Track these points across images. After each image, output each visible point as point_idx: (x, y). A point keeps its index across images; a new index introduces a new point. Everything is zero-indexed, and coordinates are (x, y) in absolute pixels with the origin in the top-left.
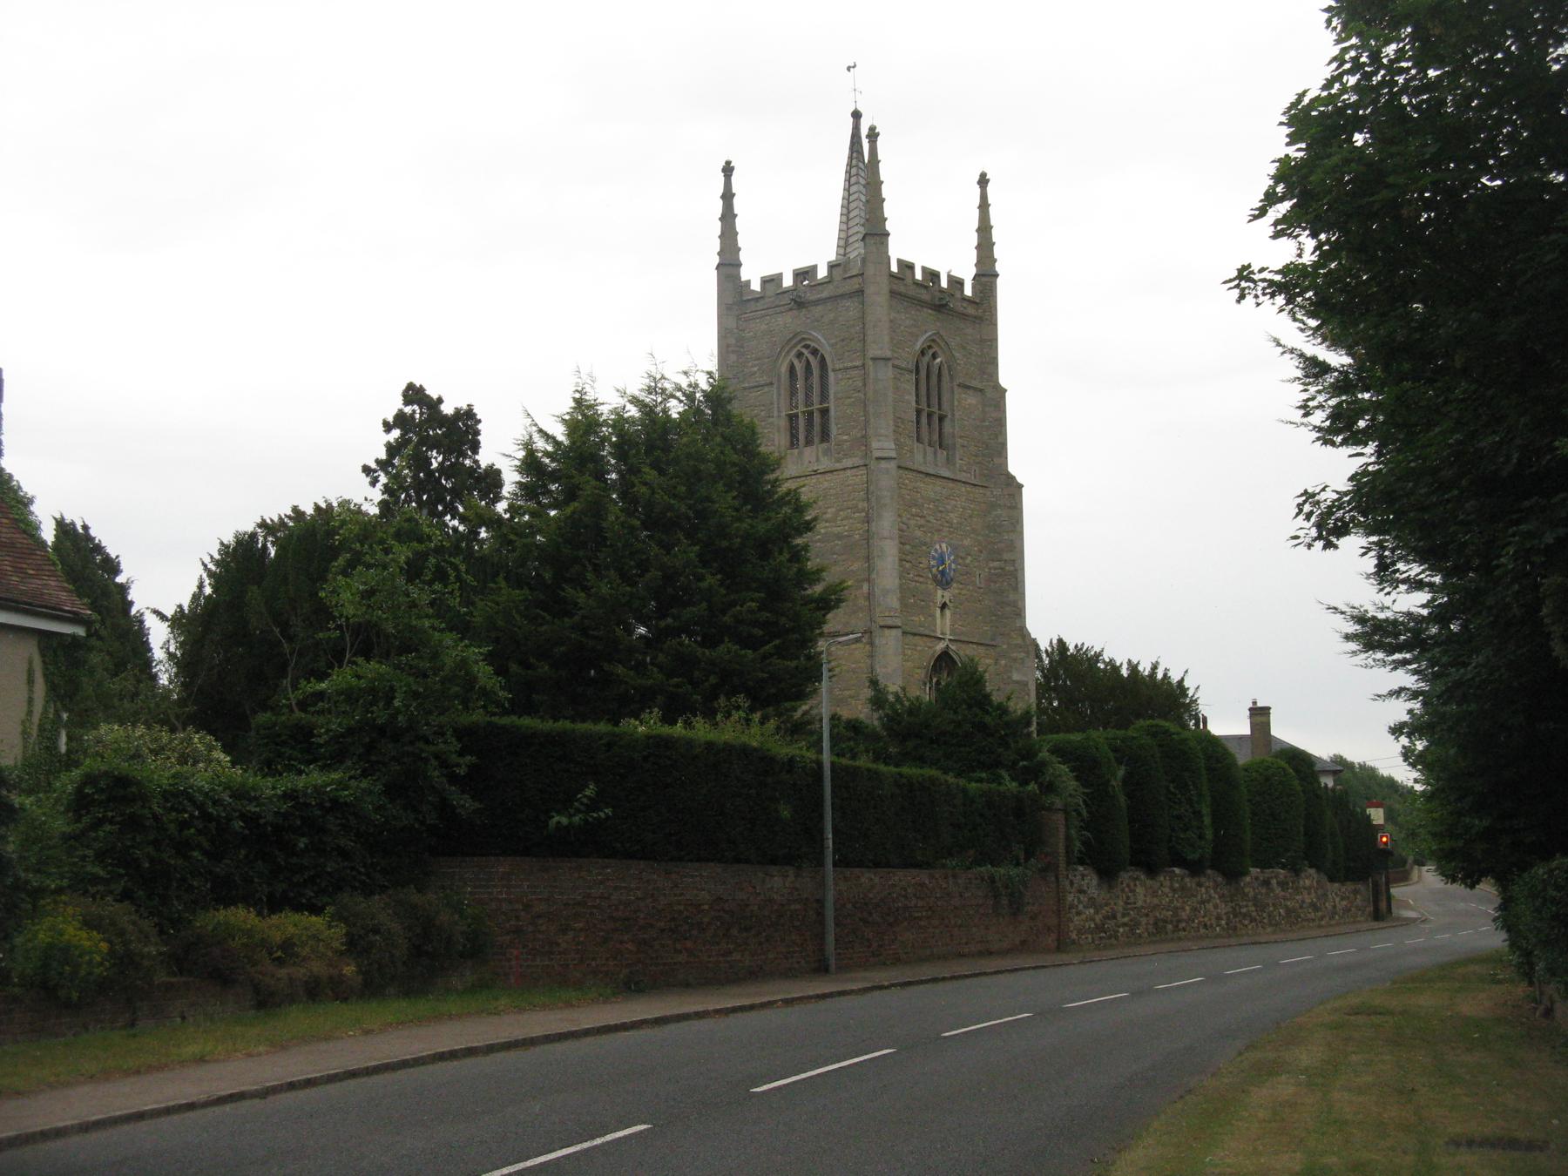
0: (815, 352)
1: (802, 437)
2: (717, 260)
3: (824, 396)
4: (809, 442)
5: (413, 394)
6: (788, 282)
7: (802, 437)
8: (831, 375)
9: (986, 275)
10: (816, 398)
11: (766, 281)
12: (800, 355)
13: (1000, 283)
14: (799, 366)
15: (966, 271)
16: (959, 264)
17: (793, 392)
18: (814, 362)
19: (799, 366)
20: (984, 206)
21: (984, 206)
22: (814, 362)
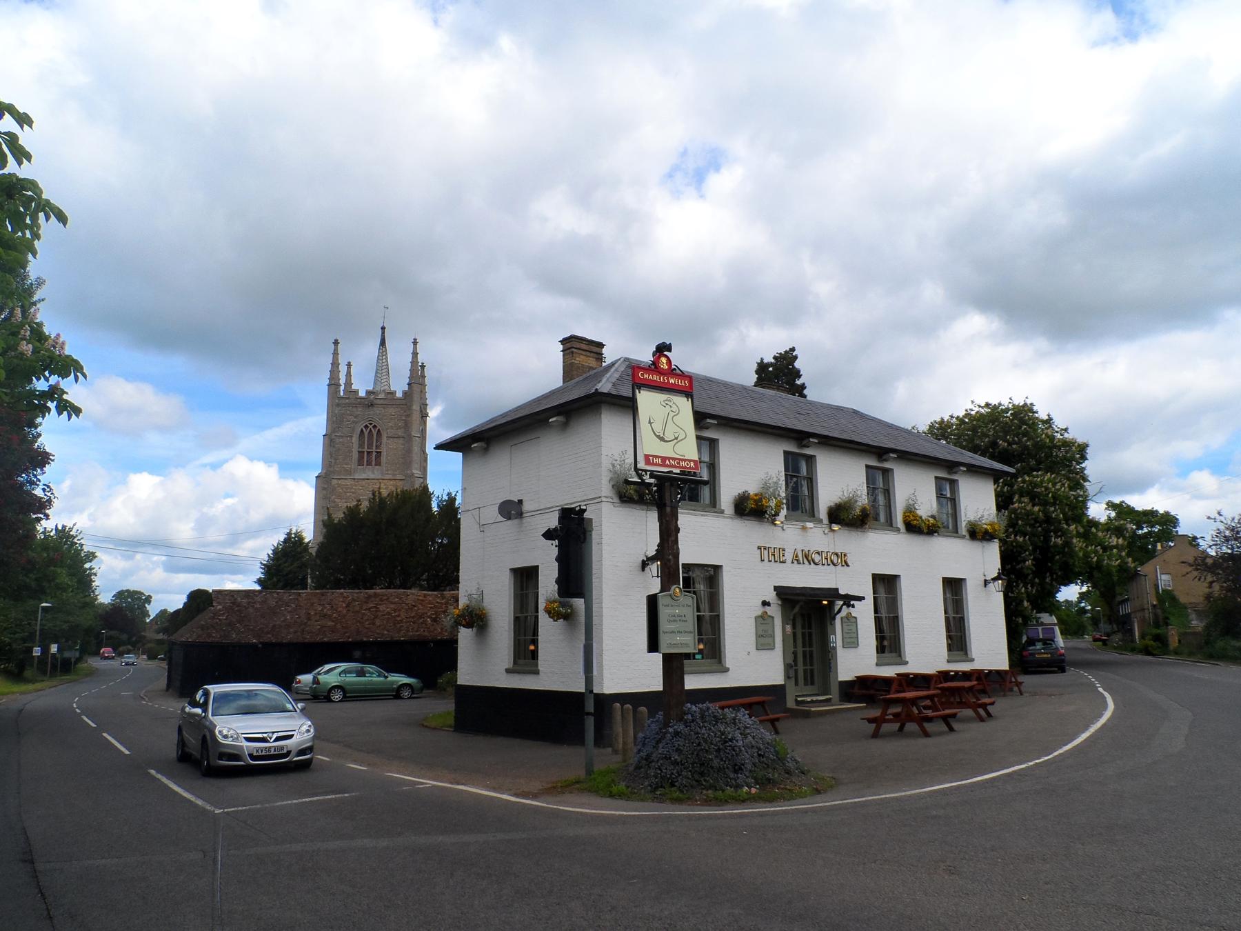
0: (375, 427)
4: (369, 464)
8: (384, 440)
14: (366, 433)
18: (375, 432)
19: (366, 433)
22: (375, 432)
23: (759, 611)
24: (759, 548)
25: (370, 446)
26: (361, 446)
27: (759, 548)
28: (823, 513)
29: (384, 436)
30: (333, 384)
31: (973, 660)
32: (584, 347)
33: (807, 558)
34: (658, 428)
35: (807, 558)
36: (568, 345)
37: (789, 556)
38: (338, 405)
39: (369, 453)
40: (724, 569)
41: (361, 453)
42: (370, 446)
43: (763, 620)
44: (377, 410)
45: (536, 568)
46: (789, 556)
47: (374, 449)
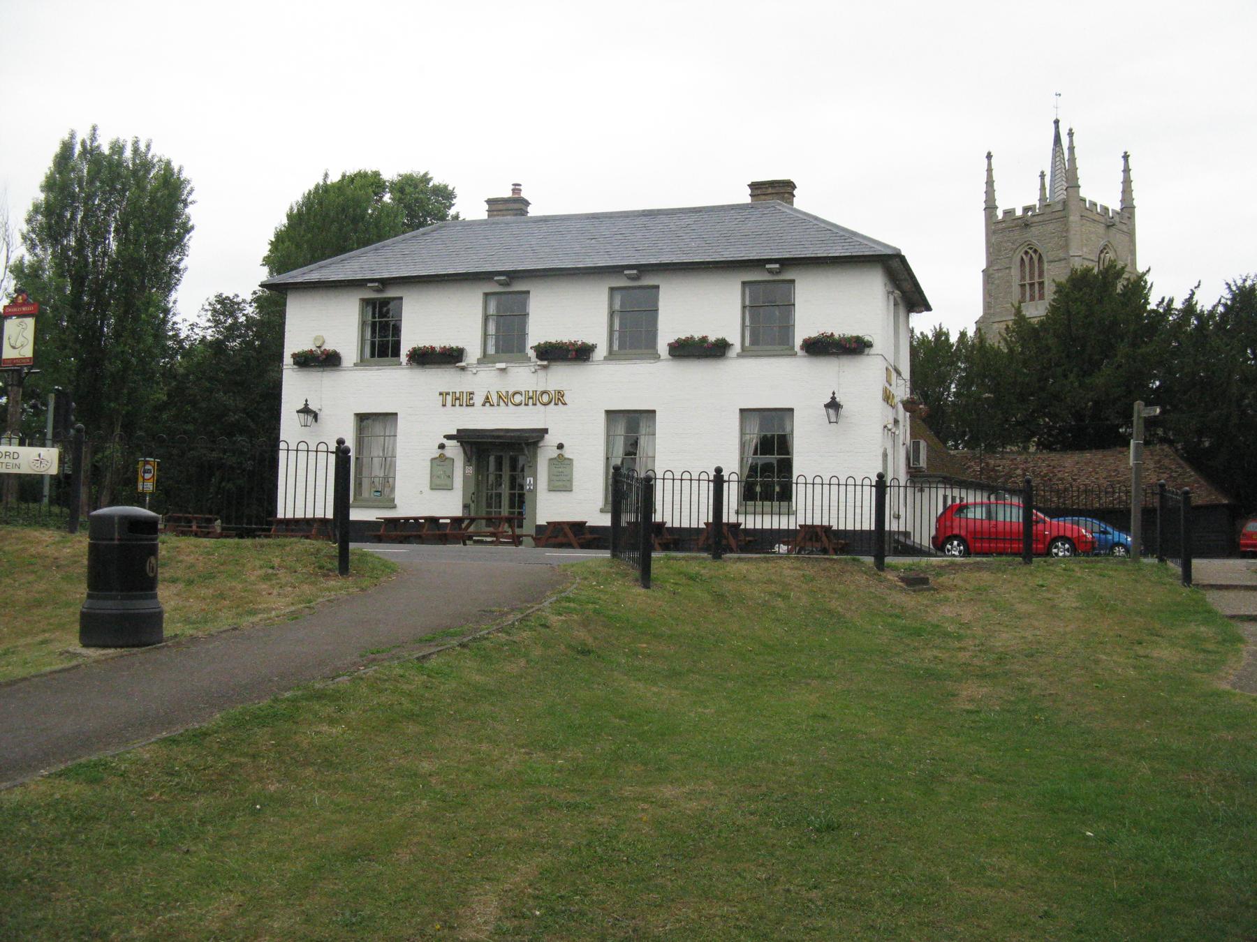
0: (1035, 251)
1: (1037, 295)
2: (984, 206)
3: (1041, 274)
4: (1032, 299)
5: (516, 188)
6: (1019, 213)
7: (1037, 295)
8: (1046, 266)
9: (1128, 208)
10: (1027, 278)
11: (1006, 213)
12: (1026, 253)
13: (1137, 212)
14: (1026, 259)
15: (1114, 204)
16: (1114, 204)
17: (1023, 271)
18: (1035, 257)
19: (1026, 259)
20: (990, 170)
21: (990, 170)
22: (1035, 257)
23: (436, 453)
24: (441, 394)
25: (1032, 277)
26: (1023, 278)
27: (441, 394)
28: (662, 348)
29: (1045, 259)
30: (990, 207)
31: (395, 507)
32: (501, 207)
33: (505, 399)
34: (12, 342)
35: (505, 399)
36: (494, 207)
37: (479, 400)
38: (994, 232)
39: (1032, 285)
40: (662, 423)
41: (1023, 286)
42: (1032, 277)
43: (441, 461)
44: (1034, 230)
45: (357, 415)
46: (479, 400)
47: (1036, 279)
